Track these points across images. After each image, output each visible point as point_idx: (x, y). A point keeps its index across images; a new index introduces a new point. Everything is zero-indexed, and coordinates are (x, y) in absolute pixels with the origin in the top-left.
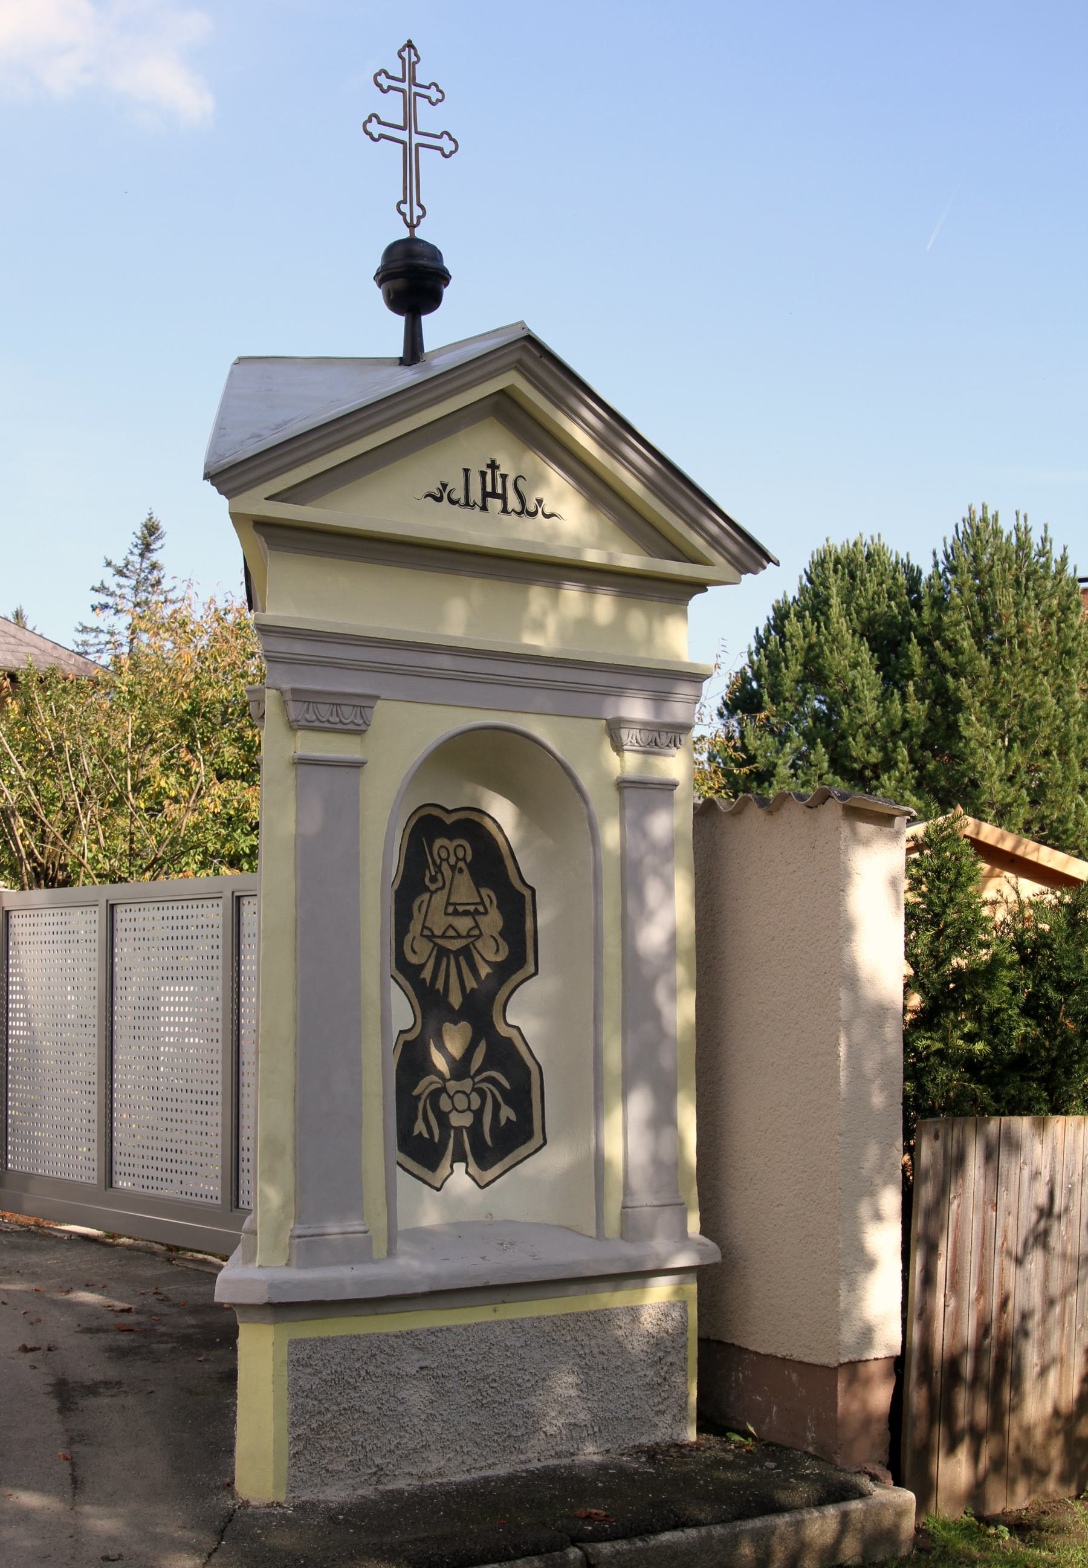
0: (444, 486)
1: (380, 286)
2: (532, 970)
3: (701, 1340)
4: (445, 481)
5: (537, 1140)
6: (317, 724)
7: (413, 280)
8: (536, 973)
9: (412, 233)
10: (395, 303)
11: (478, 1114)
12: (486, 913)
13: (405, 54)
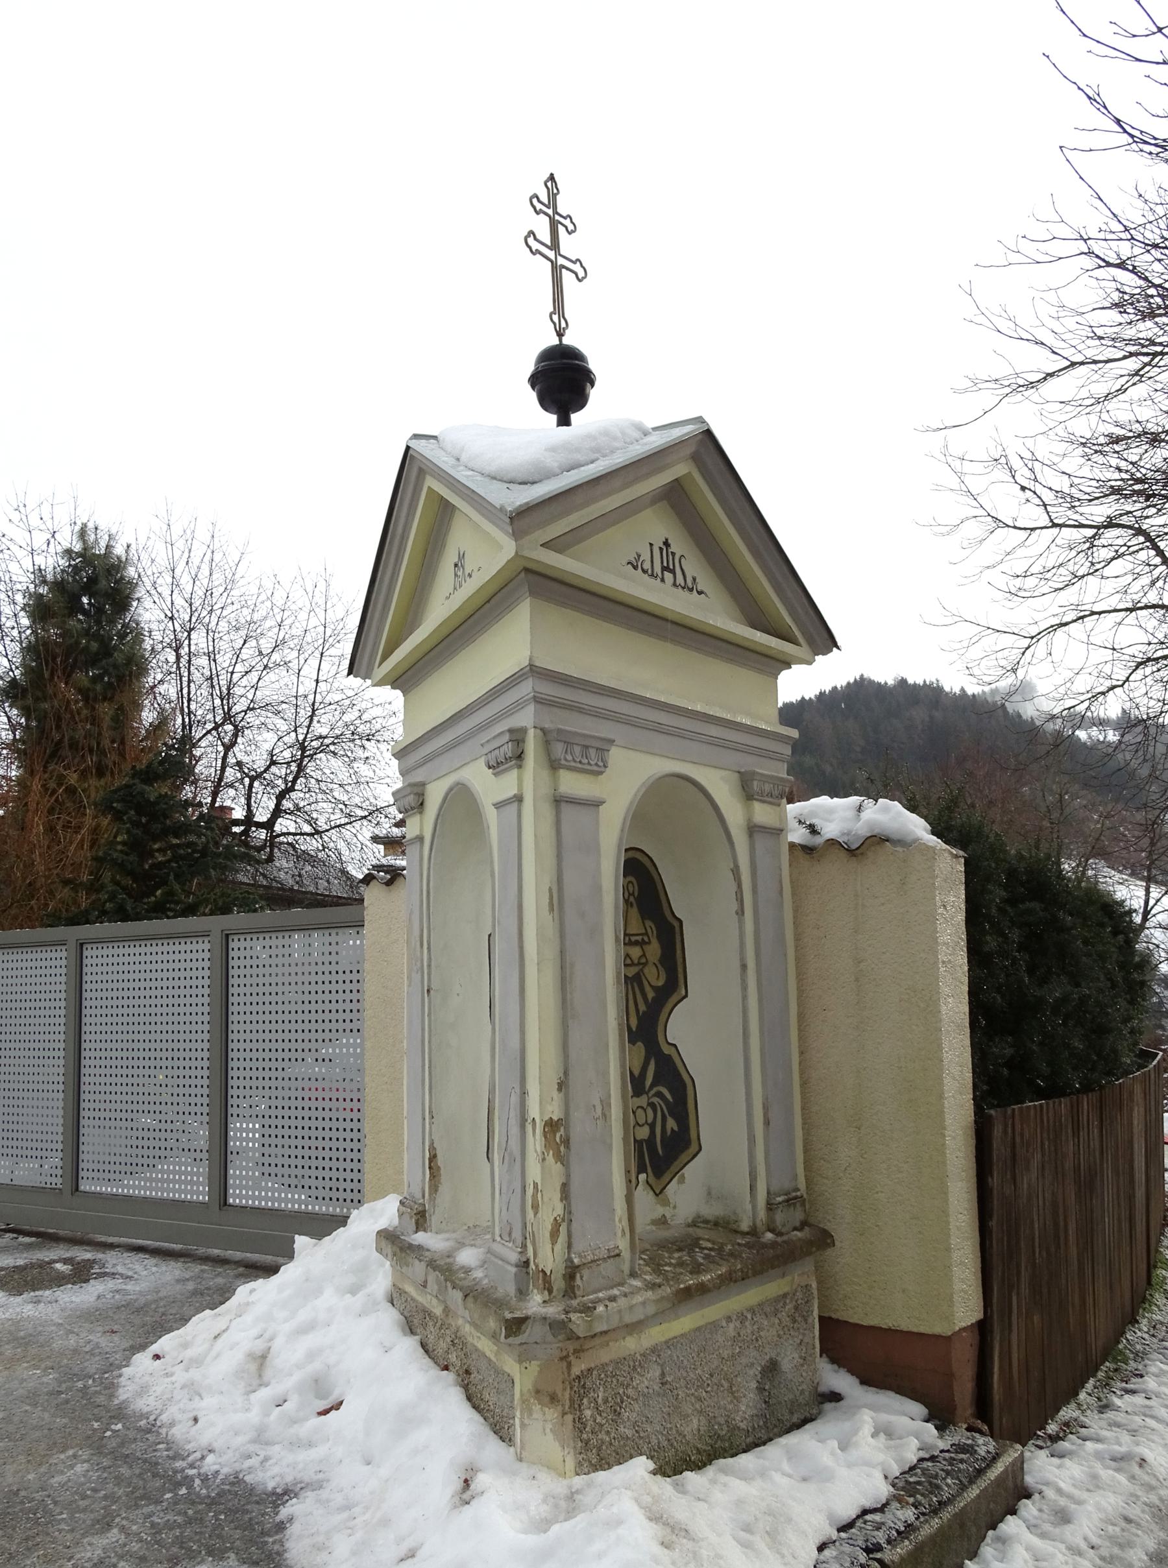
0: (639, 556)
1: (533, 387)
2: (683, 993)
3: (821, 1318)
4: (639, 552)
5: (693, 1148)
6: (573, 764)
7: (562, 381)
8: (686, 996)
9: (560, 340)
10: (546, 401)
11: (652, 1126)
12: (649, 943)
13: (549, 184)
